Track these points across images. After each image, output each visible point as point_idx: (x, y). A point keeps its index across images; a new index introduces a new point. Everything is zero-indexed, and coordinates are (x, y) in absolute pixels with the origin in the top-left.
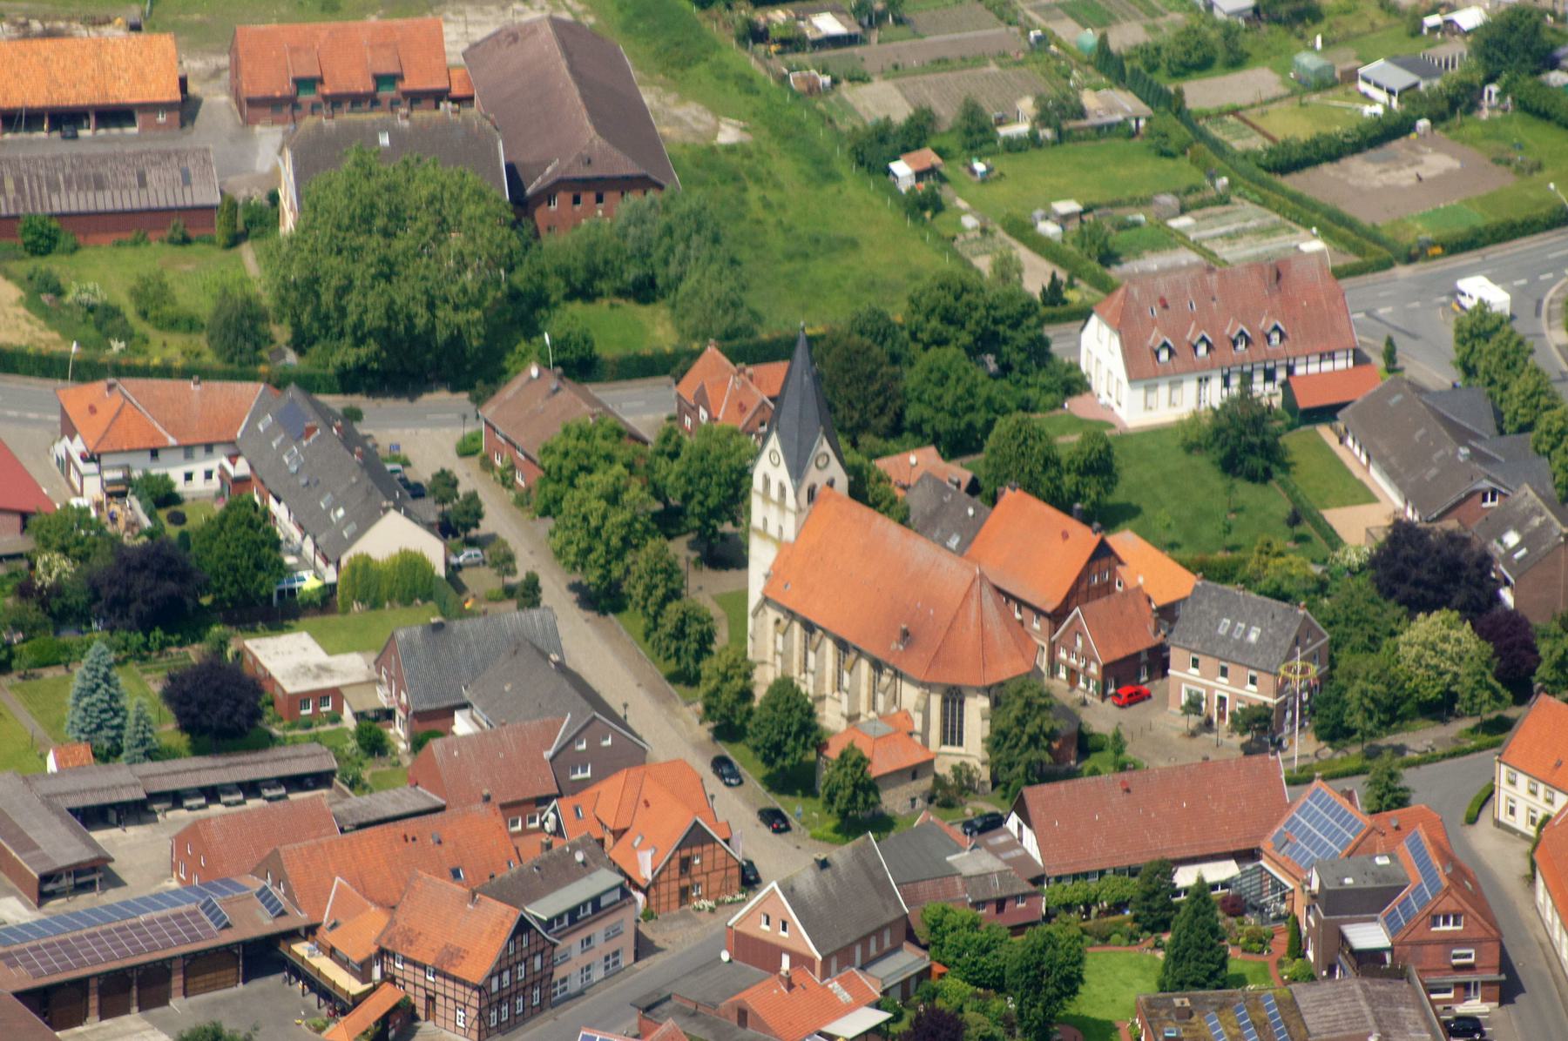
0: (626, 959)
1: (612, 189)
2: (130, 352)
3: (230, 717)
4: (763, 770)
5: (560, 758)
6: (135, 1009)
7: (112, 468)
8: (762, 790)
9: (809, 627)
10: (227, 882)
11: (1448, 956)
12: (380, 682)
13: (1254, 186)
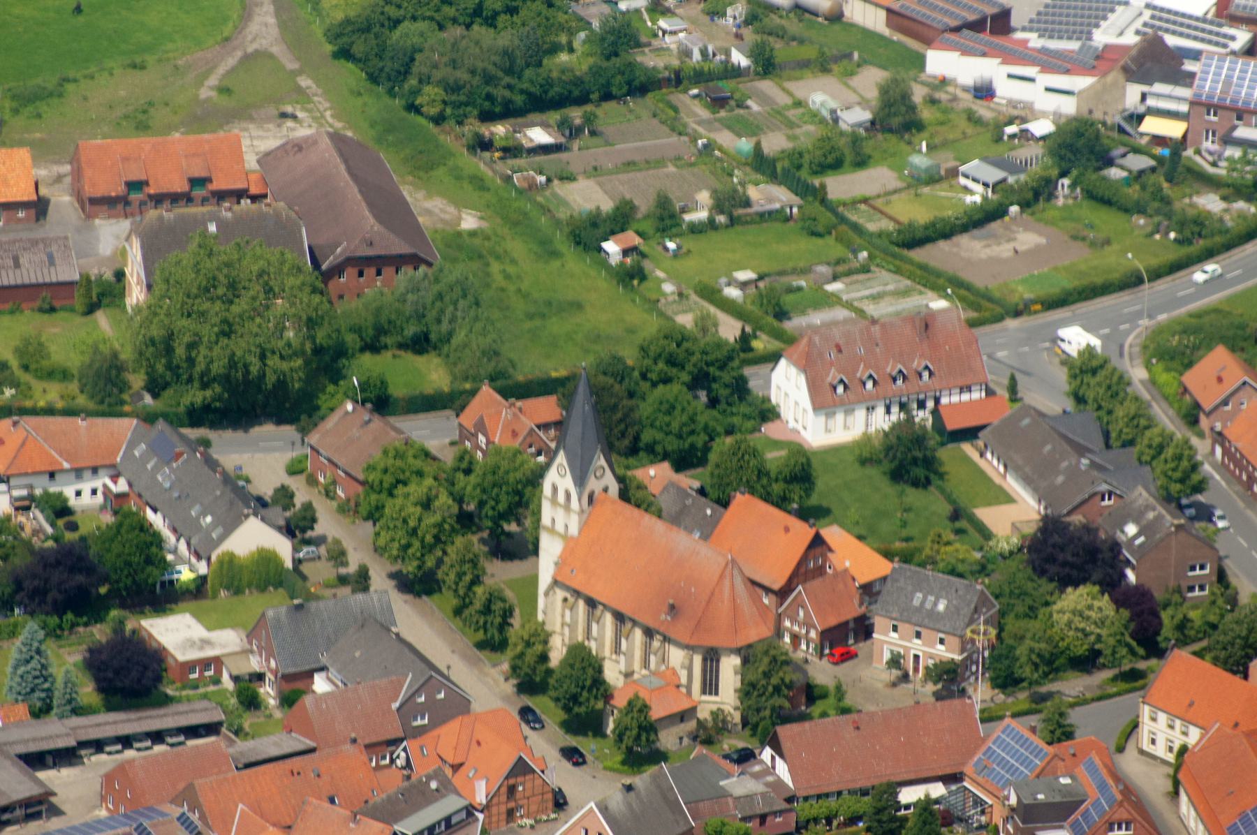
1: (390, 265)
2: (20, 396)
3: (139, 681)
4: (562, 715)
5: (405, 708)
7: (19, 487)
8: (561, 732)
9: (591, 603)
10: (151, 809)
12: (252, 652)
13: (890, 259)
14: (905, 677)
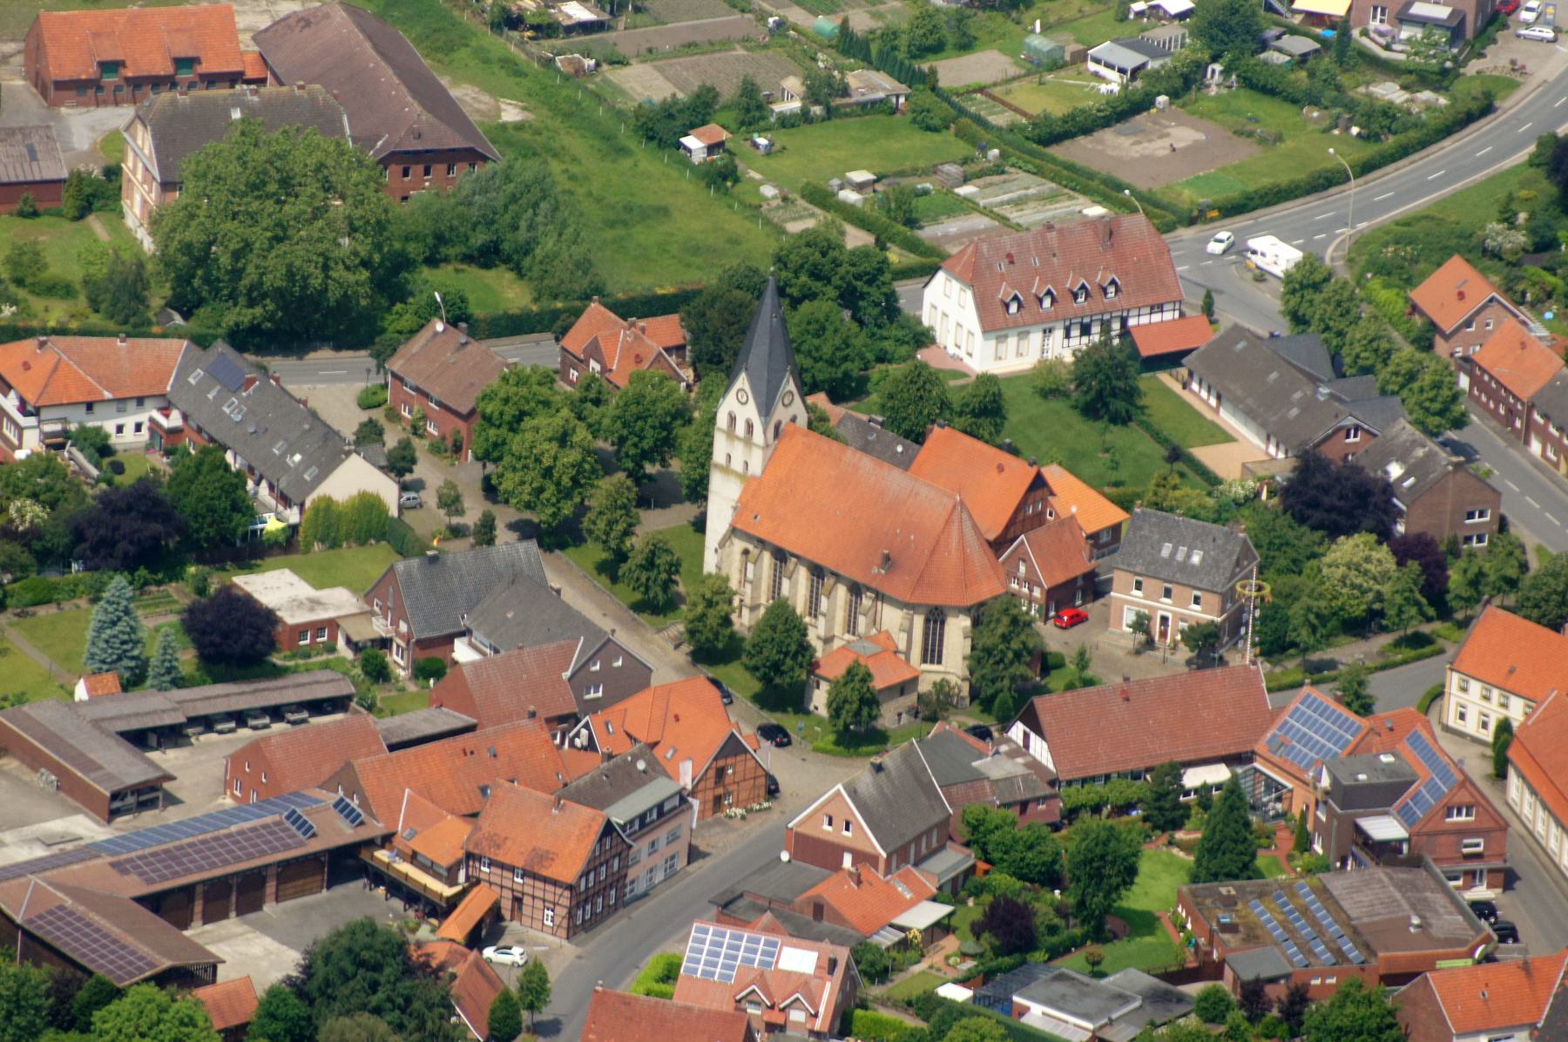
0: (681, 863)
1: (462, 160)
3: (252, 646)
4: (757, 686)
6: (233, 914)
8: (755, 708)
9: (781, 555)
11: (1460, 845)
12: (373, 614)
14: (1150, 644)
